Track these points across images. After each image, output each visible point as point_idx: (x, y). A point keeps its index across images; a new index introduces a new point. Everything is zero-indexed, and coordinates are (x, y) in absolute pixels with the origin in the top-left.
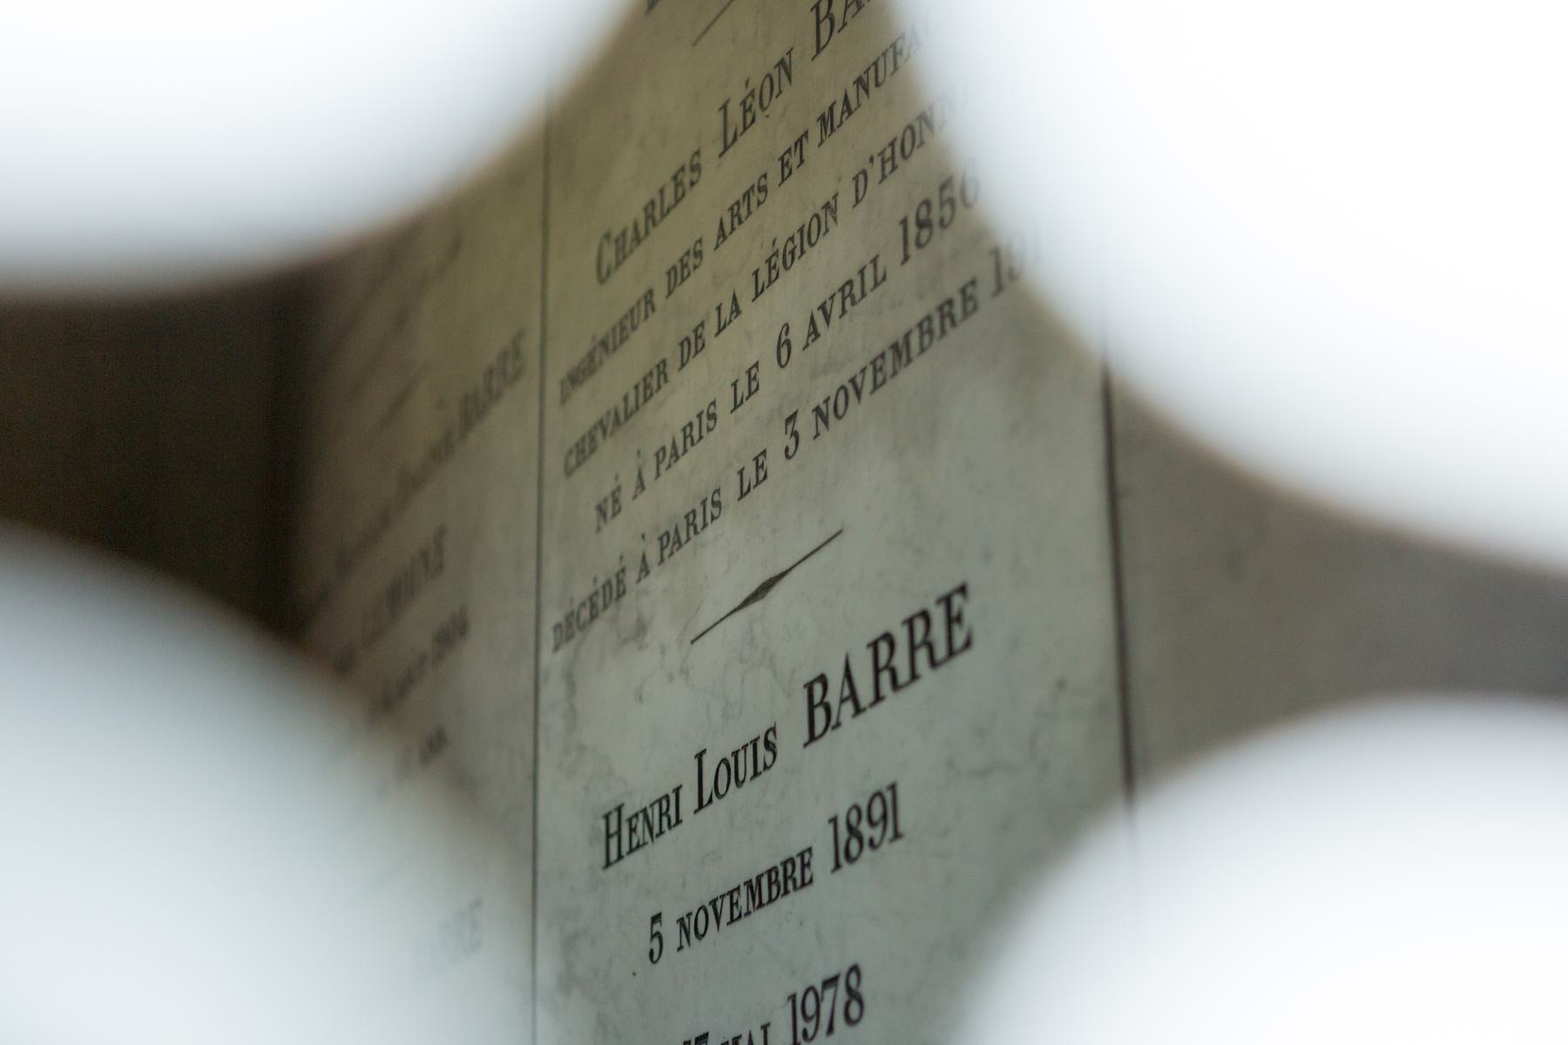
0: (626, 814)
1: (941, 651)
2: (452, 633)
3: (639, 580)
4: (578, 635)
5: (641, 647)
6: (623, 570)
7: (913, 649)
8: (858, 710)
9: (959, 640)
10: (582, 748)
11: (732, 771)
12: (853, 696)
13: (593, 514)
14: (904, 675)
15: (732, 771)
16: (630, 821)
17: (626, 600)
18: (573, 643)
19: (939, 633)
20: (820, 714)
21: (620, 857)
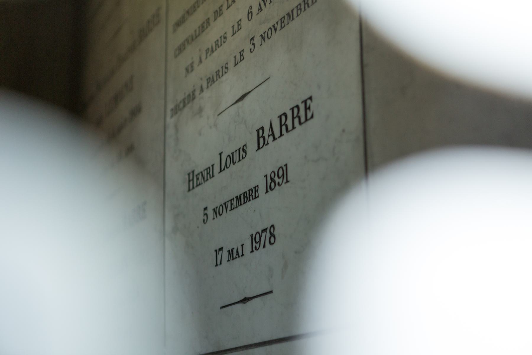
1: (303, 119)
2: (136, 111)
7: (293, 118)
8: (274, 139)
9: (309, 116)
14: (290, 127)
20: (261, 140)
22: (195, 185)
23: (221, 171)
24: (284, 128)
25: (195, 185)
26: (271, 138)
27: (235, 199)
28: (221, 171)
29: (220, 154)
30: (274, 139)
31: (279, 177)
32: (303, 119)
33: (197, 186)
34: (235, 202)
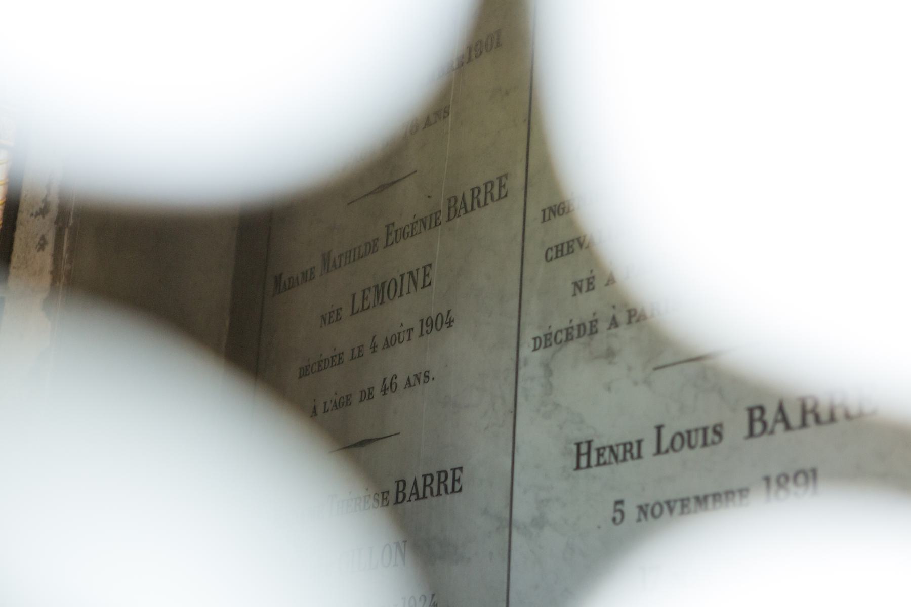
0: (595, 445)
1: (496, 197)
2: (438, 323)
3: (610, 328)
4: (554, 347)
5: (610, 363)
6: (596, 321)
7: (486, 193)
8: (466, 212)
9: (503, 194)
10: (557, 406)
11: (686, 439)
12: (465, 207)
13: (570, 288)
14: (482, 203)
15: (686, 439)
16: (598, 450)
17: (597, 337)
18: (550, 350)
19: (496, 191)
20: (453, 210)
21: (355, 249)
22: (357, 257)
23: (387, 245)
24: (476, 201)
25: (357, 257)
26: (463, 211)
27: (373, 290)
28: (387, 245)
29: (659, 428)
30: (466, 212)
31: (427, 326)
32: (496, 197)
33: (359, 258)
34: (371, 296)
